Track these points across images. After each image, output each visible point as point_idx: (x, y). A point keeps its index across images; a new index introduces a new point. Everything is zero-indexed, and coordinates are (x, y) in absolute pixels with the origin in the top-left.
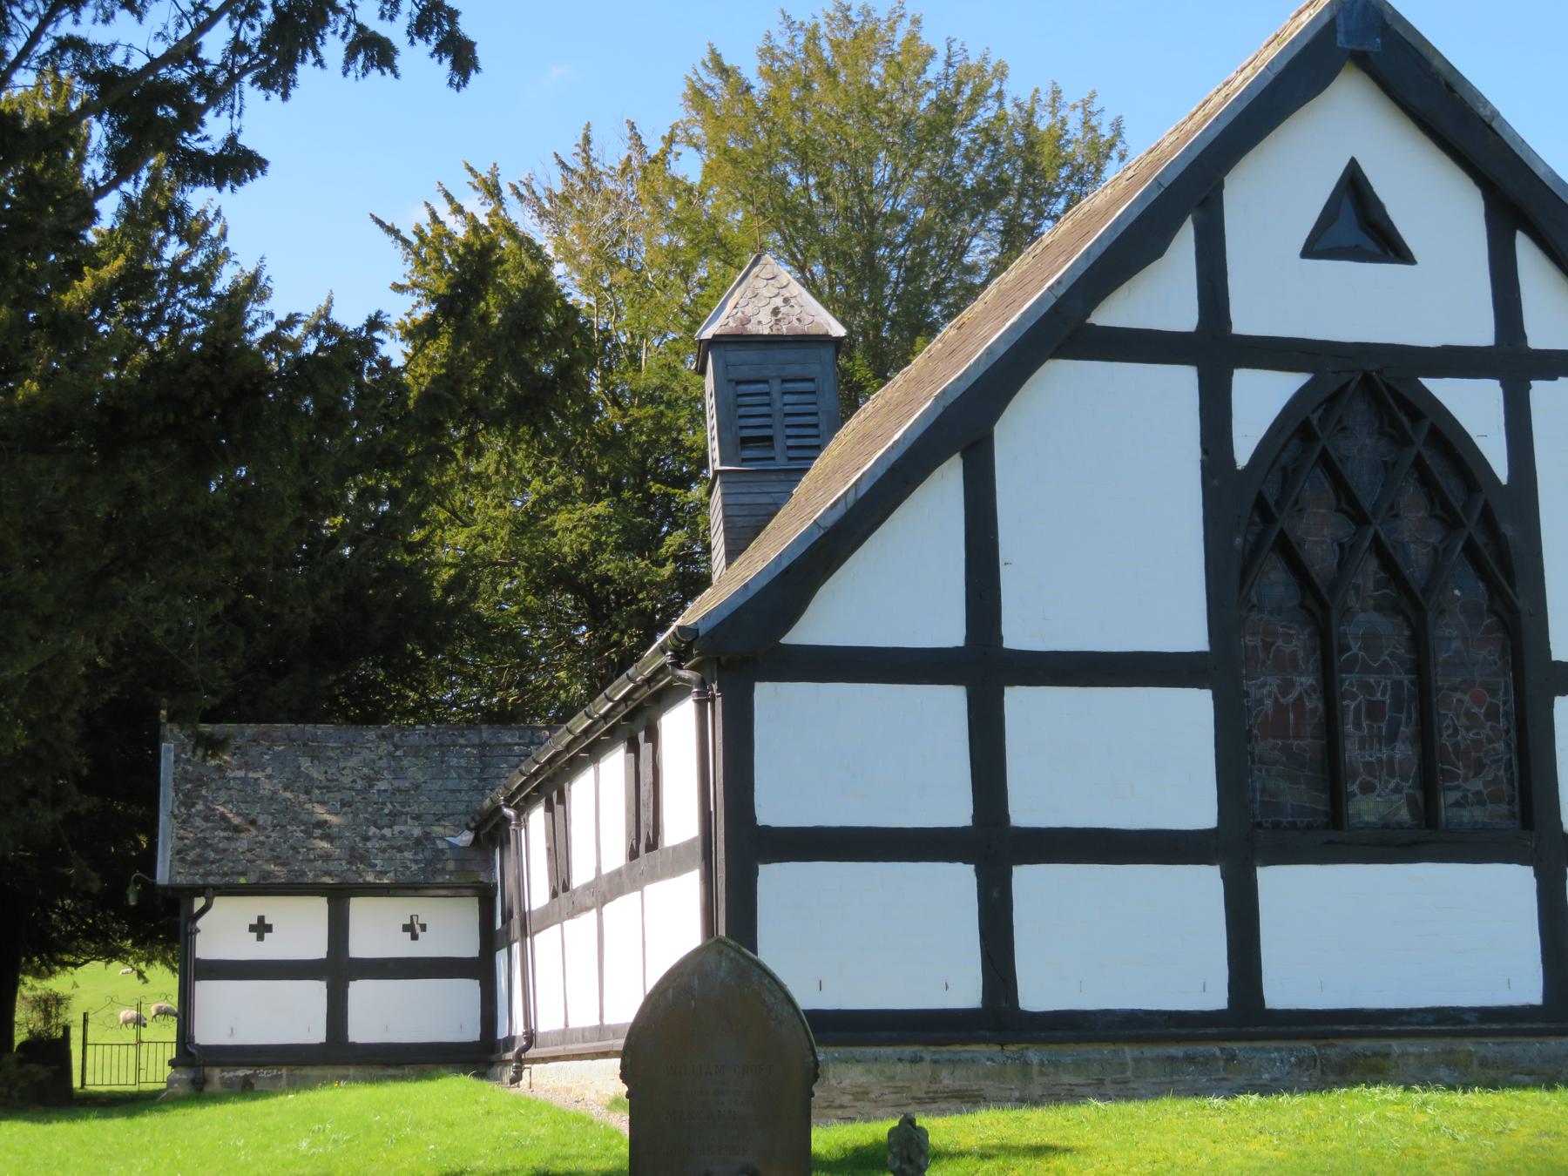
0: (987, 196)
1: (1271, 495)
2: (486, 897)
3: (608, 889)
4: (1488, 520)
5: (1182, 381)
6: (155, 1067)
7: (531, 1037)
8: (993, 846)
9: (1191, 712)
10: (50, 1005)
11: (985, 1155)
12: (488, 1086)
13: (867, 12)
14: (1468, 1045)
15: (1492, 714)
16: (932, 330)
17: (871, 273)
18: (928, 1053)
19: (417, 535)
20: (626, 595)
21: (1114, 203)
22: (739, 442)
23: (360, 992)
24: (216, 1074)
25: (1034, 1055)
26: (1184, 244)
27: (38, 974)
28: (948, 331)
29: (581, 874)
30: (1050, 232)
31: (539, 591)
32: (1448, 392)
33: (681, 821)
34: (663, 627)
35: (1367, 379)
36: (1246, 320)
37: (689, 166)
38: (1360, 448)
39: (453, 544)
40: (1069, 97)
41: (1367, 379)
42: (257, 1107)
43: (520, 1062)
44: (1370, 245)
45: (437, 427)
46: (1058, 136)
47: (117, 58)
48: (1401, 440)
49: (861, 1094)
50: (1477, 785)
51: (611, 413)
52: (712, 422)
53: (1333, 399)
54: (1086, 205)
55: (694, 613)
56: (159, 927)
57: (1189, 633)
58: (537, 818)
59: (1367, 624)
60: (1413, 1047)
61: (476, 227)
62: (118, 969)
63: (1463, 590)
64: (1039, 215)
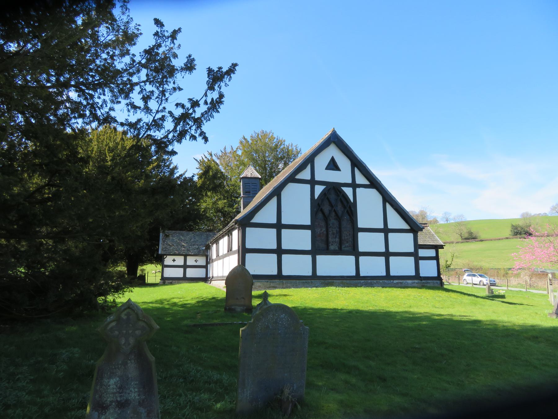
0: (282, 158)
1: (320, 203)
2: (207, 257)
3: (224, 256)
4: (350, 207)
5: (308, 187)
6: (158, 280)
7: (213, 277)
8: (279, 252)
9: (308, 234)
10: (143, 270)
11: (277, 296)
12: (206, 284)
13: (266, 132)
14: (345, 281)
15: (350, 235)
16: (274, 177)
17: (265, 169)
18: (269, 281)
19: (198, 204)
20: (229, 213)
21: (299, 161)
22: (245, 192)
23: (188, 270)
24: (167, 281)
25: (284, 281)
26: (309, 167)
27: (141, 266)
28: (276, 178)
29: (221, 254)
30: (291, 164)
31: (216, 213)
32: (345, 189)
33: (235, 247)
34: (234, 218)
35: (334, 187)
36: (317, 178)
37: (240, 152)
38: (332, 197)
39: (204, 205)
40: (294, 145)
41: (334, 187)
42: (173, 286)
43: (211, 280)
44: (335, 168)
45: (201, 191)
46: (292, 151)
47: (156, 137)
48: (338, 196)
49: (260, 287)
50: (347, 245)
51: (227, 187)
52: (242, 189)
53: (329, 190)
54: (295, 161)
55: (238, 217)
56: (159, 259)
57: (308, 222)
58: (215, 245)
59: (333, 221)
60: (337, 281)
61: (209, 160)
62: (153, 265)
63: (346, 217)
64: (289, 161)
